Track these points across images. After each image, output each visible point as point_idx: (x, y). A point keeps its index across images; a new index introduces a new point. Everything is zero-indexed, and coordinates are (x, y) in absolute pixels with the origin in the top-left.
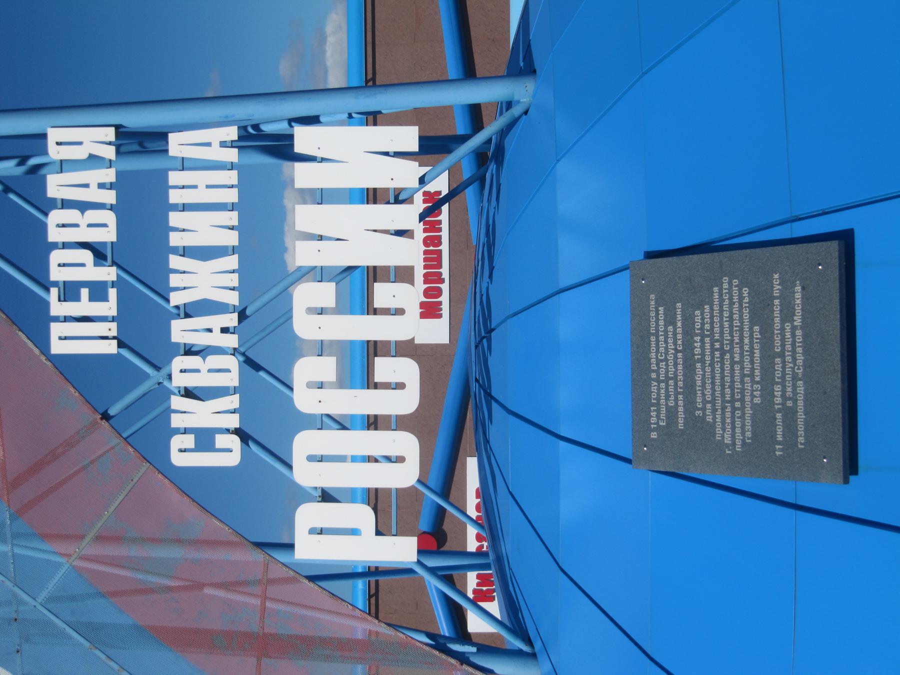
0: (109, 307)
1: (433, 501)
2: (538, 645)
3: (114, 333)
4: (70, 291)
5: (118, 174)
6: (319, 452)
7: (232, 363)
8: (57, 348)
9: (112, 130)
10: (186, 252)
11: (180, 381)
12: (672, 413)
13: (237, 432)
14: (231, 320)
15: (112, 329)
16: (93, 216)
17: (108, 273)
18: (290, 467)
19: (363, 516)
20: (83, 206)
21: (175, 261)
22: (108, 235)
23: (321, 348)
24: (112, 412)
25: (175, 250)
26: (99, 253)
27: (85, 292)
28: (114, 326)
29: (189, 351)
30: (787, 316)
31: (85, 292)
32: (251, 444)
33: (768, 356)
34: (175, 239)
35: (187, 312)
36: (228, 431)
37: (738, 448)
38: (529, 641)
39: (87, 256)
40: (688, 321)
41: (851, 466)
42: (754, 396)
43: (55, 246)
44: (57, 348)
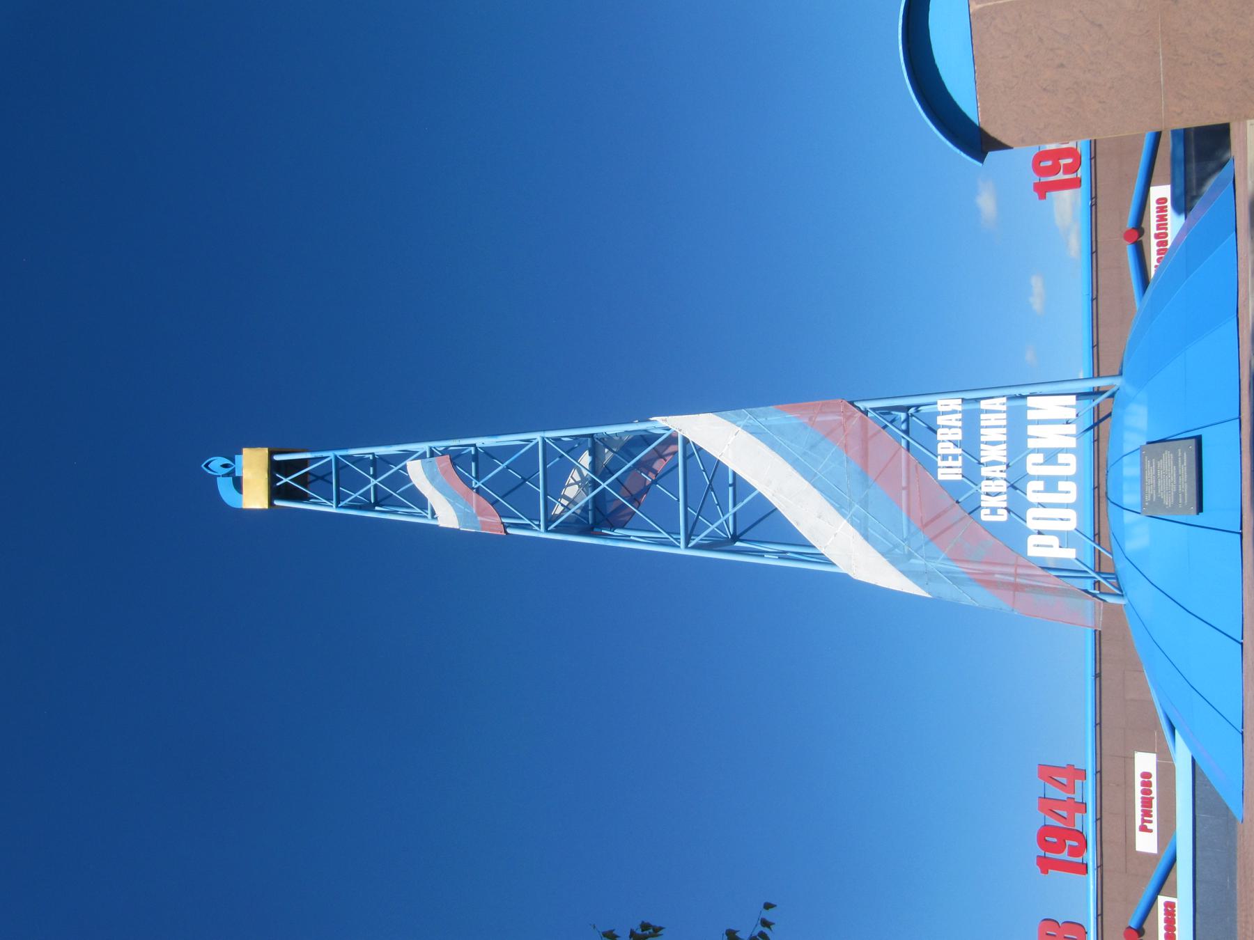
0: (959, 463)
1: (1091, 545)
2: (1124, 593)
3: (961, 472)
4: (945, 457)
5: (1008, 407)
6: (1037, 516)
7: (1005, 484)
8: (940, 477)
9: (961, 400)
10: (986, 443)
11: (984, 489)
12: (1152, 496)
13: (1006, 508)
14: (1004, 467)
15: (960, 471)
16: (953, 430)
17: (959, 451)
18: (1026, 522)
19: (1054, 541)
20: (950, 427)
21: (983, 446)
22: (959, 437)
23: (1039, 478)
24: (960, 501)
25: (983, 443)
26: (955, 444)
27: (950, 458)
28: (961, 469)
29: (988, 479)
30: (1183, 463)
31: (950, 458)
32: (1011, 513)
33: (1178, 475)
34: (983, 439)
35: (988, 464)
36: (1002, 508)
37: (1170, 506)
38: (1121, 591)
39: (951, 445)
40: (1156, 466)
41: (1200, 509)
42: (1174, 489)
43: (940, 441)
44: (940, 477)
